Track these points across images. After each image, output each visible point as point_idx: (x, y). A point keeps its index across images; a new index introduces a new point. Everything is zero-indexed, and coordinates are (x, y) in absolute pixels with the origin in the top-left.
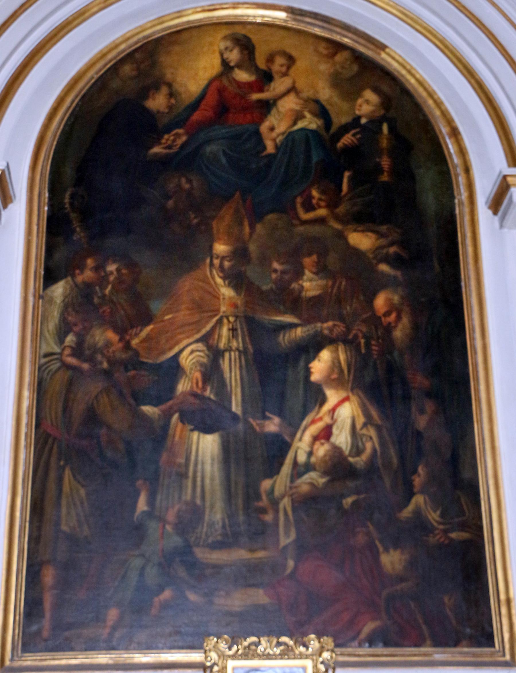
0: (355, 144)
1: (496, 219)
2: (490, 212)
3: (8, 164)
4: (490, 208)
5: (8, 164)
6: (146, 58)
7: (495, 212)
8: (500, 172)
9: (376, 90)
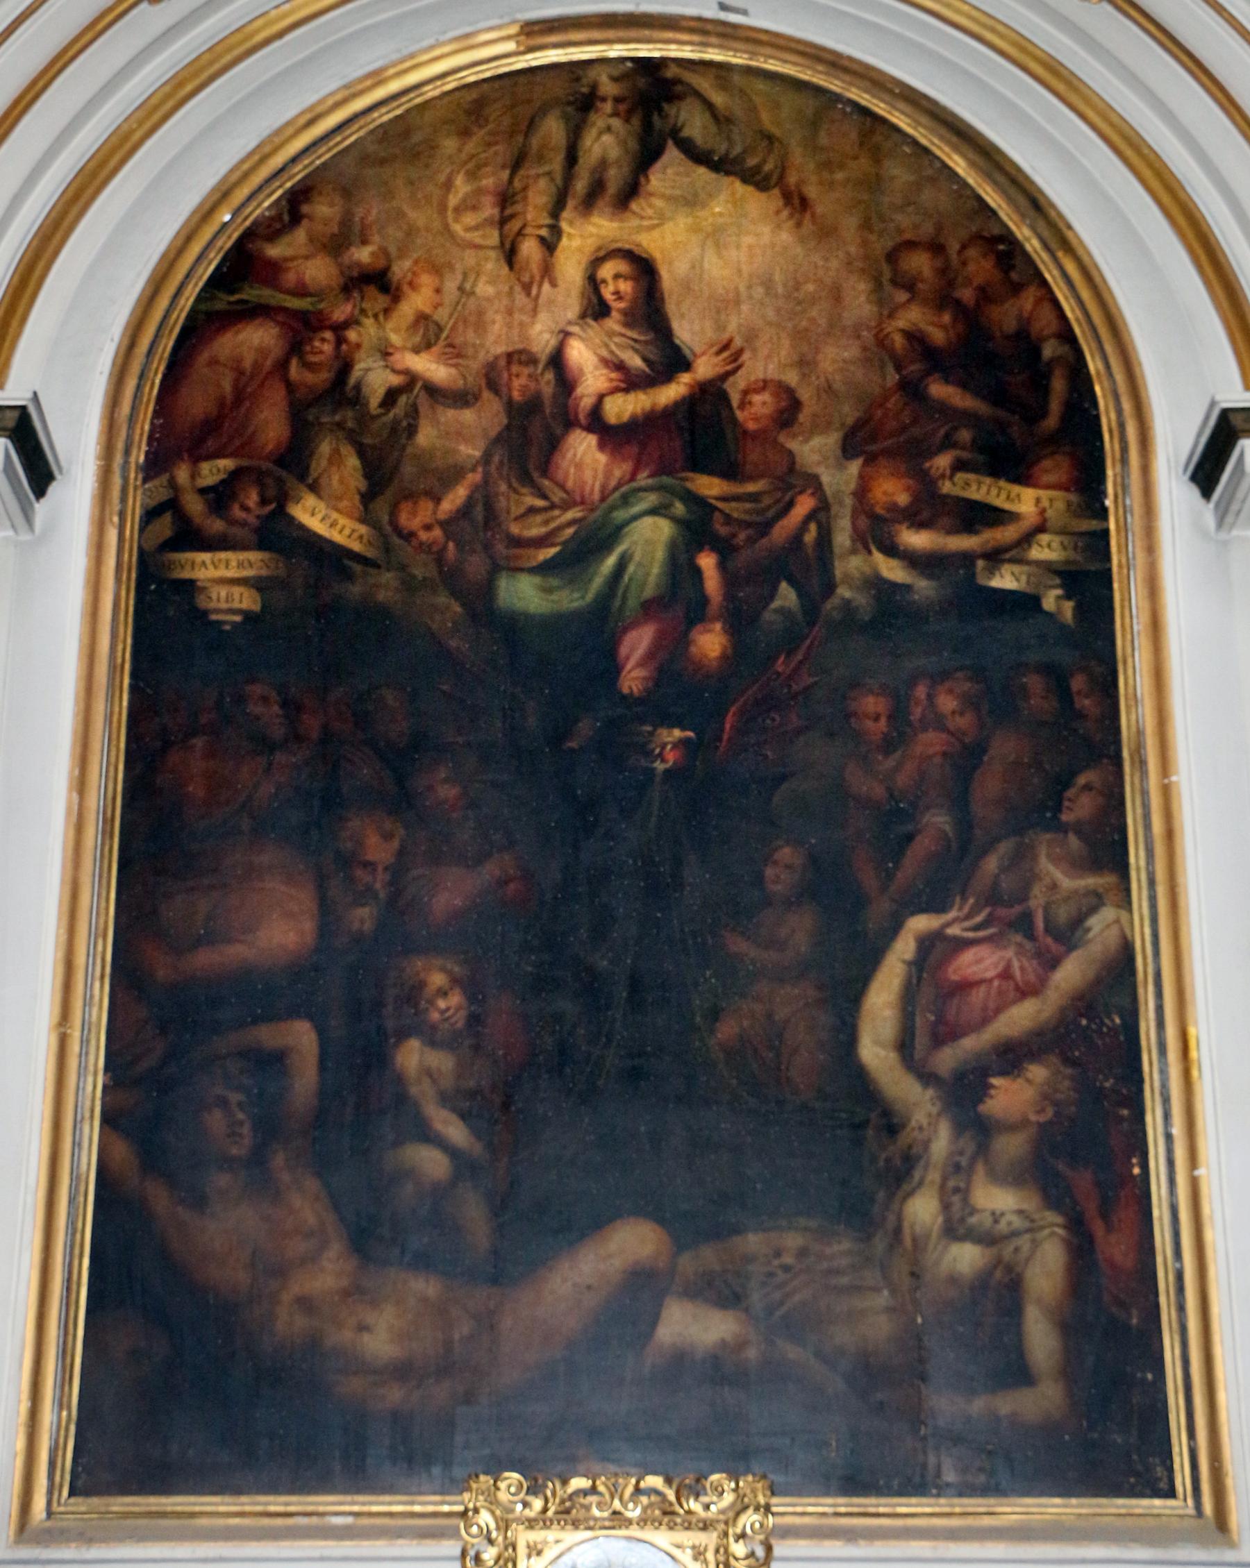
0: (644, 678)
1: (1208, 512)
2: (1194, 492)
3: (35, 394)
4: (1194, 478)
5: (35, 394)
6: (259, 351)
7: (1207, 492)
8: (1213, 404)
9: (443, 969)
